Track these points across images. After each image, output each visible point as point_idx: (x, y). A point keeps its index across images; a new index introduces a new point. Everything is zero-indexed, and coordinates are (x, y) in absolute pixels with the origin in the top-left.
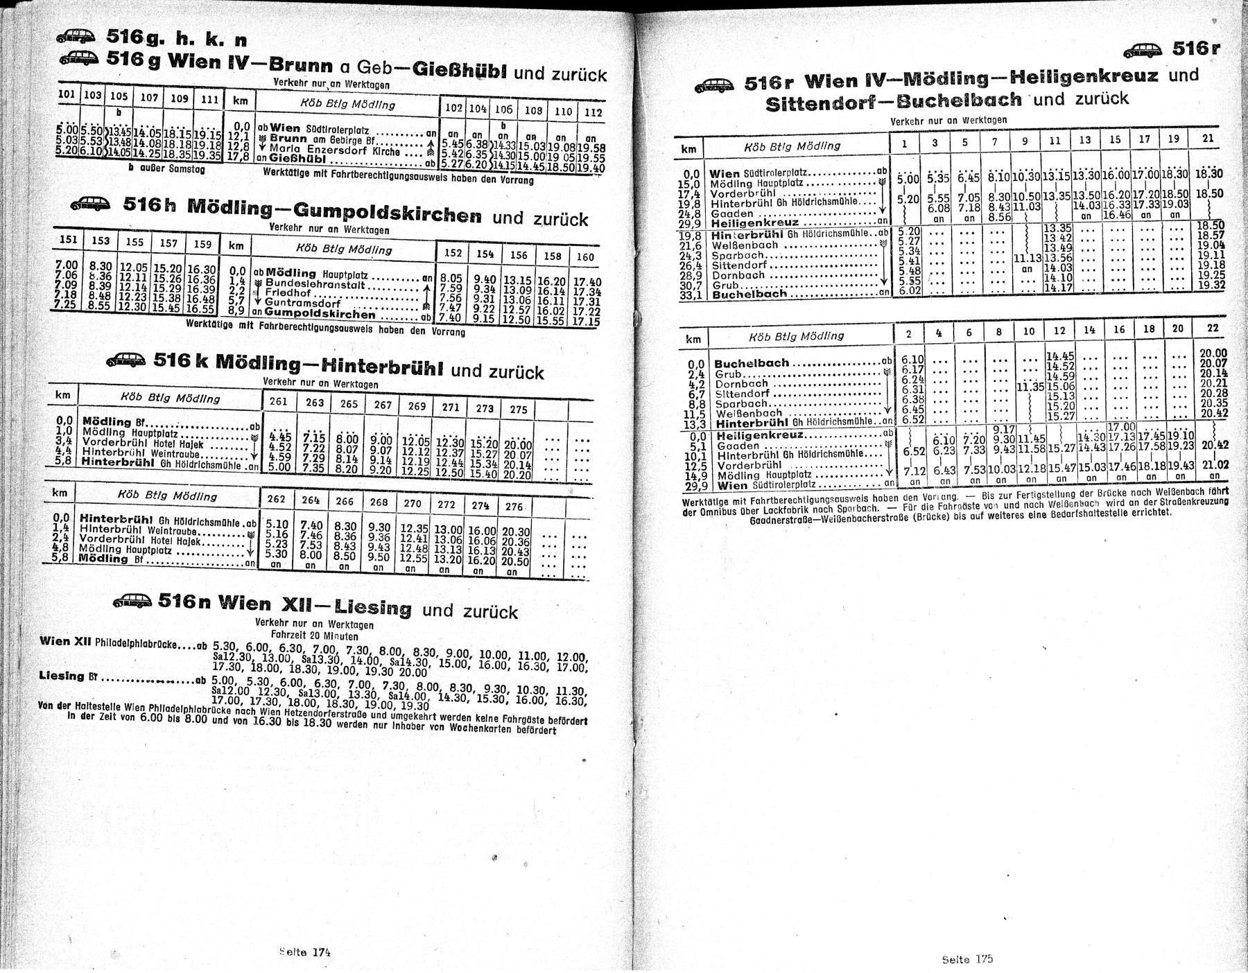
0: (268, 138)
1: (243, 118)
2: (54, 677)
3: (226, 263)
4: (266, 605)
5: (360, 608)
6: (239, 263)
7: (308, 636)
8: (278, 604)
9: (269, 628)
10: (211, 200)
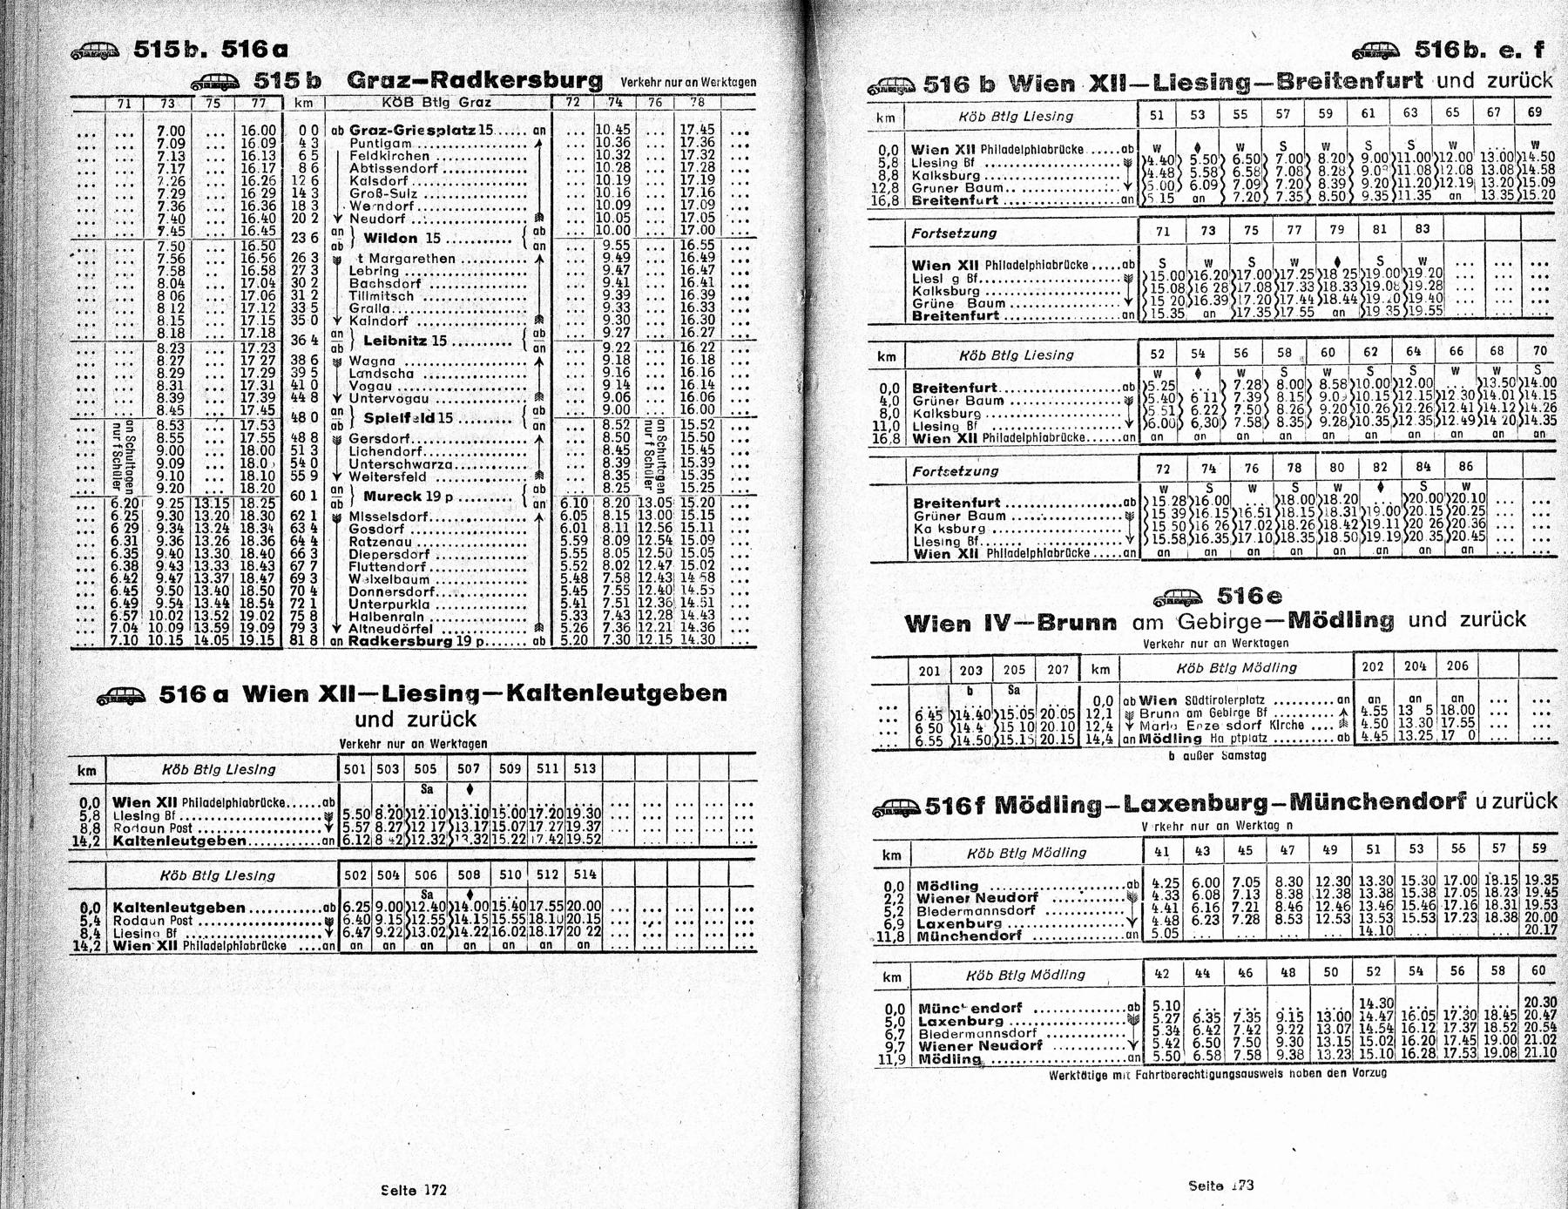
0: (1137, 715)
1: (1104, 691)
10: (1023, 797)
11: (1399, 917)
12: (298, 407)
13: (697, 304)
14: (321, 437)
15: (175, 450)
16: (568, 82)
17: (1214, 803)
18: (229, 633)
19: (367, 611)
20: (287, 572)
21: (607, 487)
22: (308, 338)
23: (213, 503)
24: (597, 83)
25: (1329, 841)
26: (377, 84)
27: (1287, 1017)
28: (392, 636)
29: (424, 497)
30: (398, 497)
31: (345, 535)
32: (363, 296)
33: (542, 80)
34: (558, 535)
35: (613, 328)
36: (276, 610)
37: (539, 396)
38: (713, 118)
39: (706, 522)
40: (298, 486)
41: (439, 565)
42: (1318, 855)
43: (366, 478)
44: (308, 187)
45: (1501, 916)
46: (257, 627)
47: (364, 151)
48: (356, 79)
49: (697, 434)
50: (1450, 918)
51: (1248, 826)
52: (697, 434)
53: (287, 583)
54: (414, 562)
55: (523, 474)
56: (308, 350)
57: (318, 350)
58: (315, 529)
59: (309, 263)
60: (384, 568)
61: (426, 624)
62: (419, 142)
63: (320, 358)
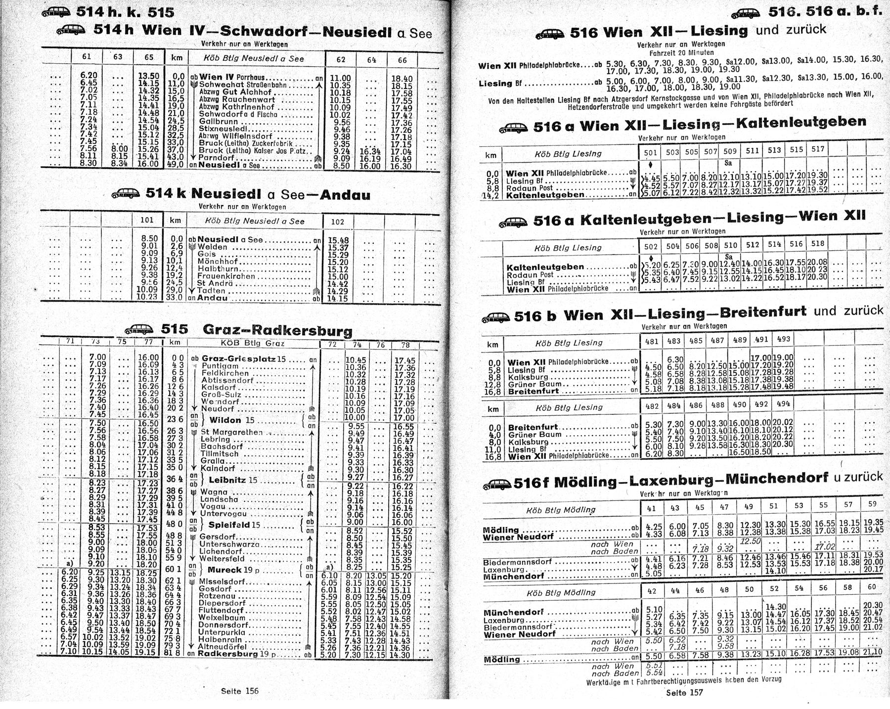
2: (490, 84)
3: (168, 234)
4: (639, 32)
5: (710, 32)
6: (177, 233)
7: (677, 53)
8: (648, 32)
9: (647, 50)
11: (789, 563)
12: (171, 518)
13: (403, 461)
14: (183, 536)
15: (99, 541)
16: (332, 332)
17: (682, 481)
18: (129, 648)
19: (209, 636)
20: (163, 613)
21: (349, 566)
22: (177, 478)
23: (121, 572)
24: (349, 333)
25: (748, 502)
26: (221, 332)
27: (724, 615)
28: (224, 651)
29: (243, 570)
30: (228, 570)
31: (197, 592)
32: (209, 454)
33: (317, 331)
34: (319, 593)
35: (354, 474)
36: (157, 634)
37: (311, 513)
38: (415, 354)
39: (406, 587)
40: (170, 563)
41: (252, 609)
42: (741, 509)
43: (209, 559)
44: (177, 391)
45: (850, 561)
46: (145, 645)
47: (210, 370)
48: (208, 329)
49: (402, 536)
50: (819, 563)
51: (702, 494)
52: (402, 536)
53: (163, 619)
54: (236, 608)
55: (300, 558)
56: (177, 485)
57: (182, 485)
58: (179, 589)
59: (177, 434)
60: (219, 611)
61: (242, 644)
62: (243, 366)
63: (184, 490)
